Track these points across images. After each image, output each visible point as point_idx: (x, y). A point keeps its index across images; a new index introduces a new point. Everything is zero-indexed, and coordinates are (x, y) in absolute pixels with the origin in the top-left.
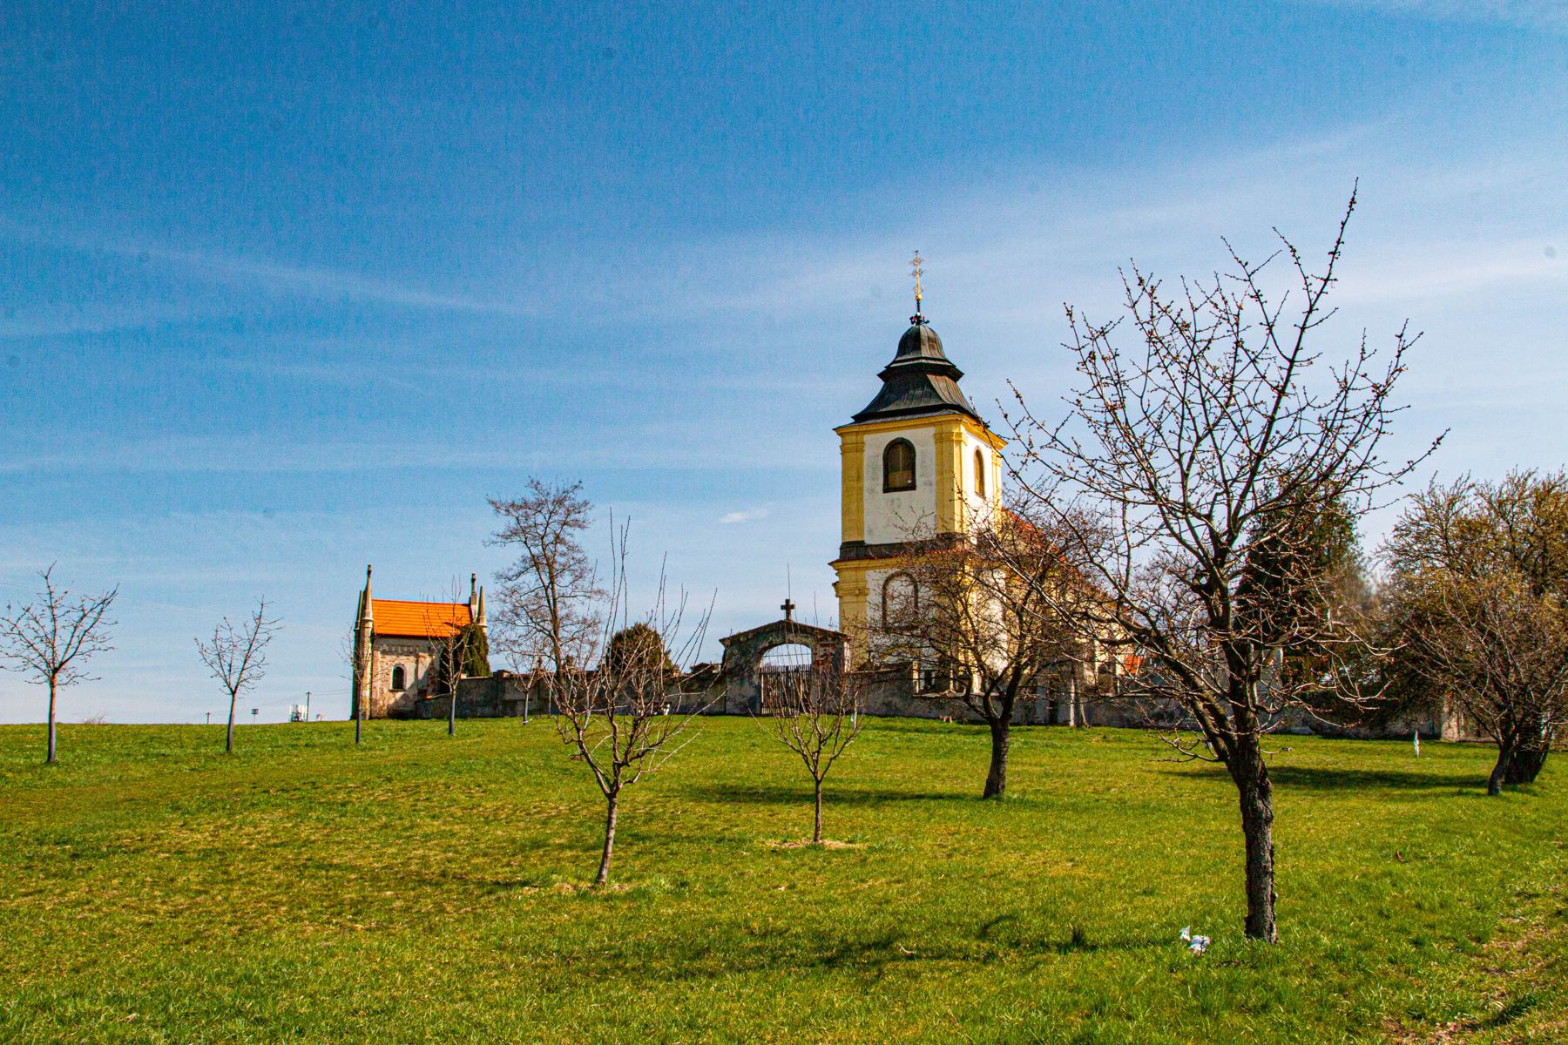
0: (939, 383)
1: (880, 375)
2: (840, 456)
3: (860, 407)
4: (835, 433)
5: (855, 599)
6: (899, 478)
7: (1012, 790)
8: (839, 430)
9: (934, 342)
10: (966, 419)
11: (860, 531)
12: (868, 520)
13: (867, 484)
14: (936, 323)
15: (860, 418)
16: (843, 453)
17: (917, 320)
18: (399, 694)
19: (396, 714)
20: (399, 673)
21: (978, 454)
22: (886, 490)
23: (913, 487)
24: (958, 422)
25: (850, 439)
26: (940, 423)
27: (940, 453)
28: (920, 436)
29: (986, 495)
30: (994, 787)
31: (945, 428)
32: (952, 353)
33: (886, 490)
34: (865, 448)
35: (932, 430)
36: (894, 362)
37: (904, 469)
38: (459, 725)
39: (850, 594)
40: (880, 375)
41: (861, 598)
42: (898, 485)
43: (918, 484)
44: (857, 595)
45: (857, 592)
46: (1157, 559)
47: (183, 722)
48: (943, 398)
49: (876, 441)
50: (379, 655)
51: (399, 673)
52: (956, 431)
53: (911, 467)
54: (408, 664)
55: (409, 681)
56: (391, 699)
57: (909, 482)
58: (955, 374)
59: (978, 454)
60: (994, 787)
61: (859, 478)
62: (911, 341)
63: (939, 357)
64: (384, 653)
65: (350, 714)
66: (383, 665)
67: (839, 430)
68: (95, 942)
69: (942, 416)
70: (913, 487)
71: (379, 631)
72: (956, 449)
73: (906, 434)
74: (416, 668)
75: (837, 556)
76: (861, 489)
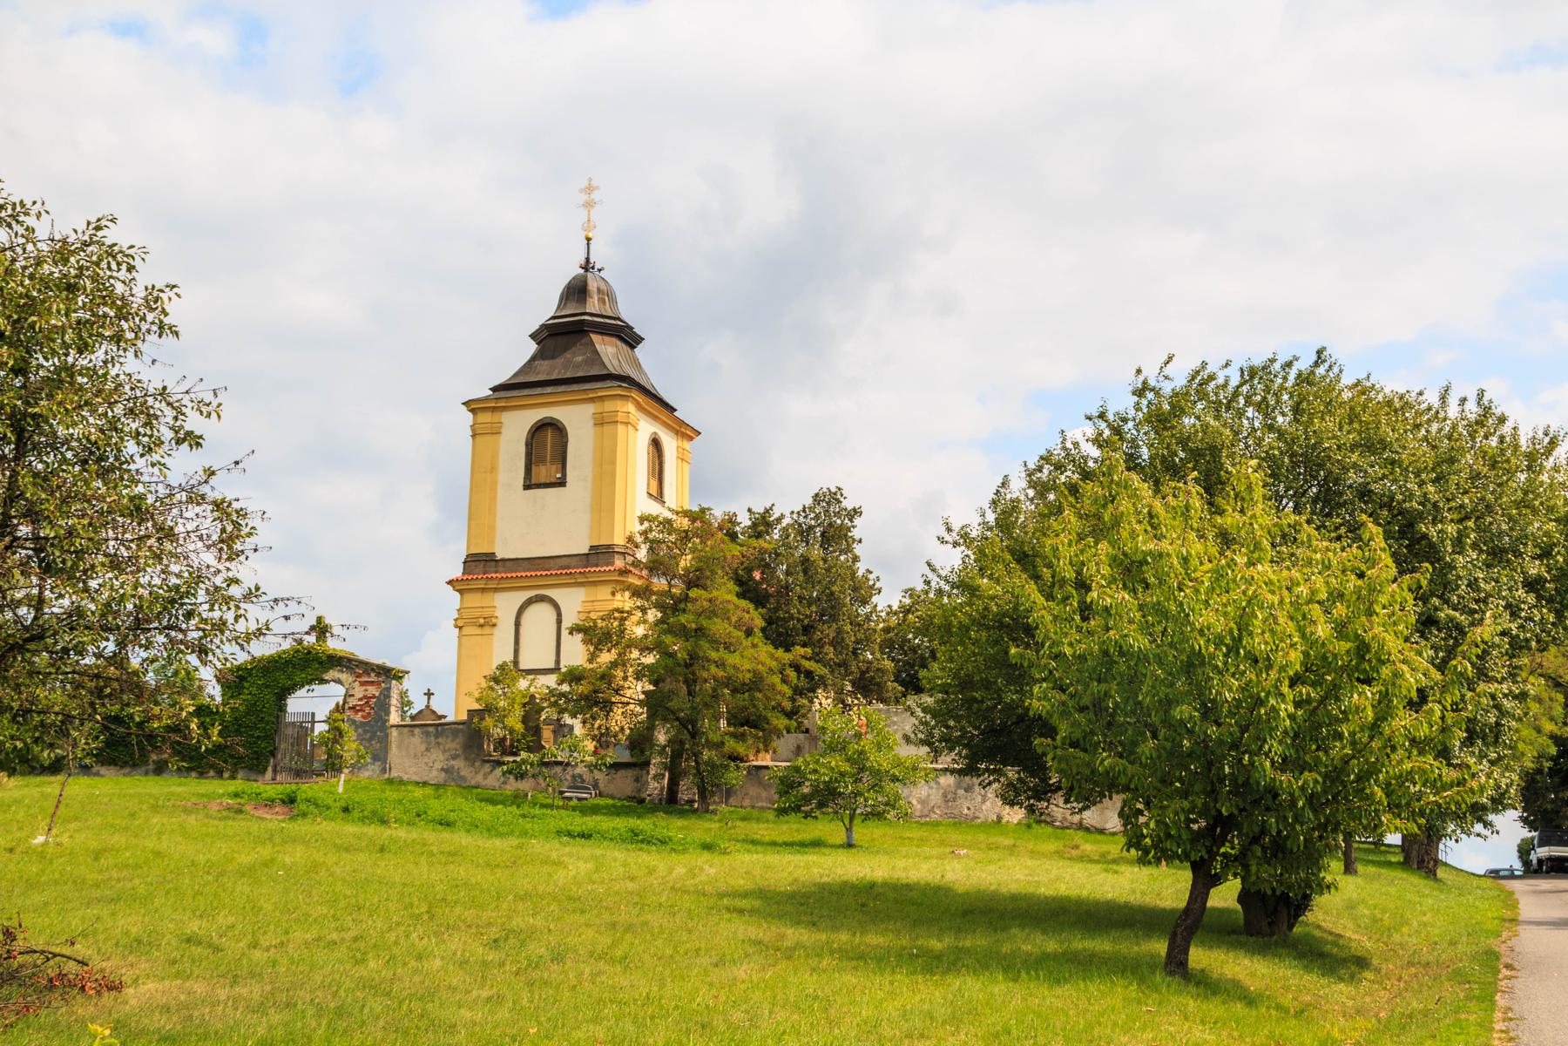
0: (609, 351)
1: (533, 336)
3: (503, 377)
4: (464, 408)
5: (478, 631)
6: (543, 472)
8: (473, 406)
9: (607, 295)
10: (635, 394)
13: (502, 477)
16: (473, 436)
17: (587, 266)
21: (656, 443)
22: (527, 487)
23: (561, 483)
25: (485, 417)
26: (602, 398)
28: (576, 417)
29: (666, 498)
33: (527, 487)
34: (503, 430)
36: (554, 318)
37: (552, 463)
39: (473, 624)
40: (533, 336)
41: (487, 630)
43: (568, 479)
44: (481, 626)
45: (482, 621)
46: (1432, 398)
47: (548, 676)
48: (610, 367)
49: (518, 424)
53: (562, 459)
57: (559, 475)
58: (629, 338)
59: (656, 443)
61: (493, 469)
62: (576, 291)
63: (610, 314)
67: (473, 406)
68: (1082, 552)
70: (561, 483)
73: (556, 413)
75: (457, 572)
76: (494, 484)
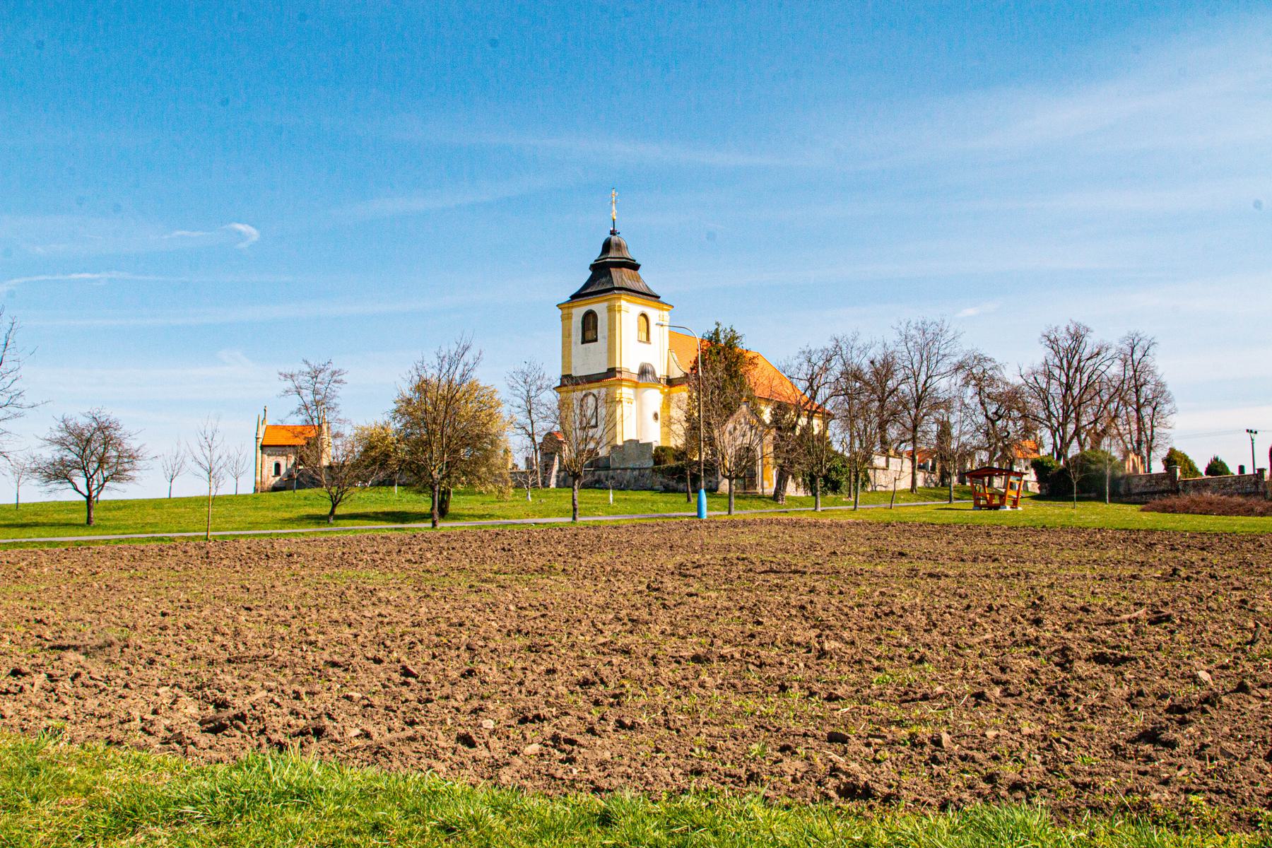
2: (560, 323)
7: (95, 522)
11: (570, 368)
12: (574, 364)
14: (624, 238)
15: (574, 297)
18: (278, 478)
19: (275, 489)
20: (278, 466)
22: (583, 343)
23: (596, 340)
24: (619, 299)
27: (610, 316)
28: (599, 307)
30: (89, 521)
31: (612, 302)
32: (632, 253)
33: (583, 343)
35: (606, 304)
38: (297, 491)
42: (590, 339)
49: (579, 312)
50: (265, 456)
51: (278, 466)
52: (617, 304)
54: (282, 461)
55: (283, 471)
56: (273, 481)
58: (635, 267)
60: (89, 521)
61: (569, 335)
64: (269, 455)
65: (1178, 449)
66: (270, 462)
69: (609, 296)
70: (596, 340)
71: (265, 443)
72: (618, 316)
74: (286, 463)
76: (570, 342)
